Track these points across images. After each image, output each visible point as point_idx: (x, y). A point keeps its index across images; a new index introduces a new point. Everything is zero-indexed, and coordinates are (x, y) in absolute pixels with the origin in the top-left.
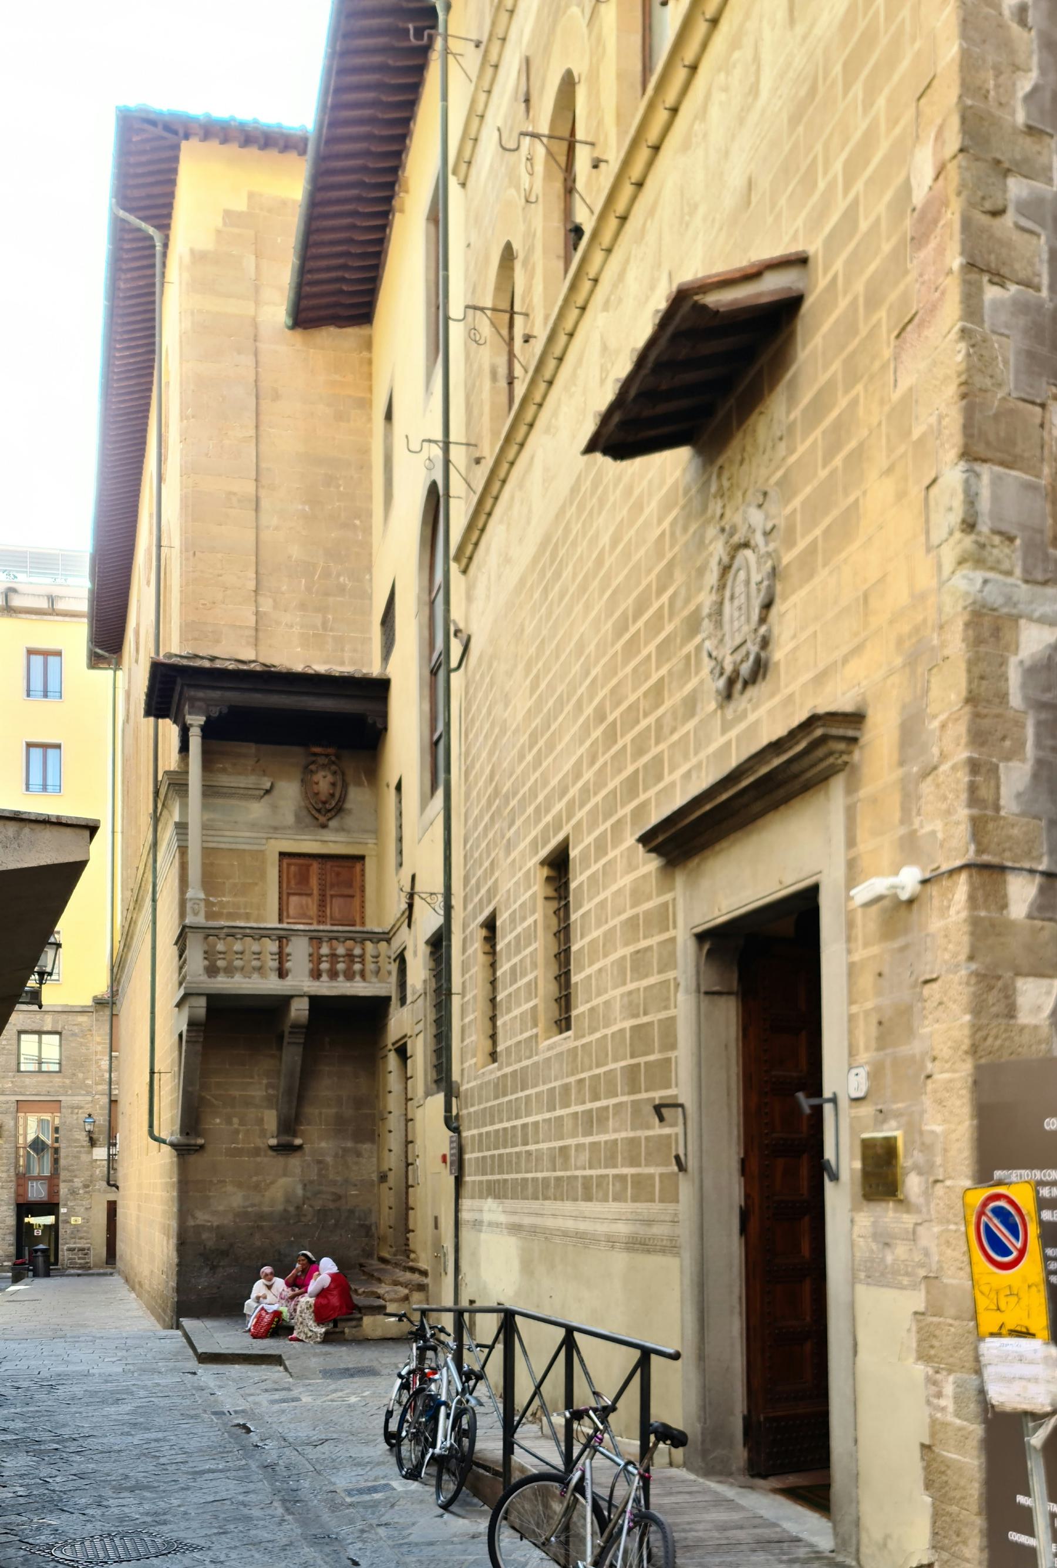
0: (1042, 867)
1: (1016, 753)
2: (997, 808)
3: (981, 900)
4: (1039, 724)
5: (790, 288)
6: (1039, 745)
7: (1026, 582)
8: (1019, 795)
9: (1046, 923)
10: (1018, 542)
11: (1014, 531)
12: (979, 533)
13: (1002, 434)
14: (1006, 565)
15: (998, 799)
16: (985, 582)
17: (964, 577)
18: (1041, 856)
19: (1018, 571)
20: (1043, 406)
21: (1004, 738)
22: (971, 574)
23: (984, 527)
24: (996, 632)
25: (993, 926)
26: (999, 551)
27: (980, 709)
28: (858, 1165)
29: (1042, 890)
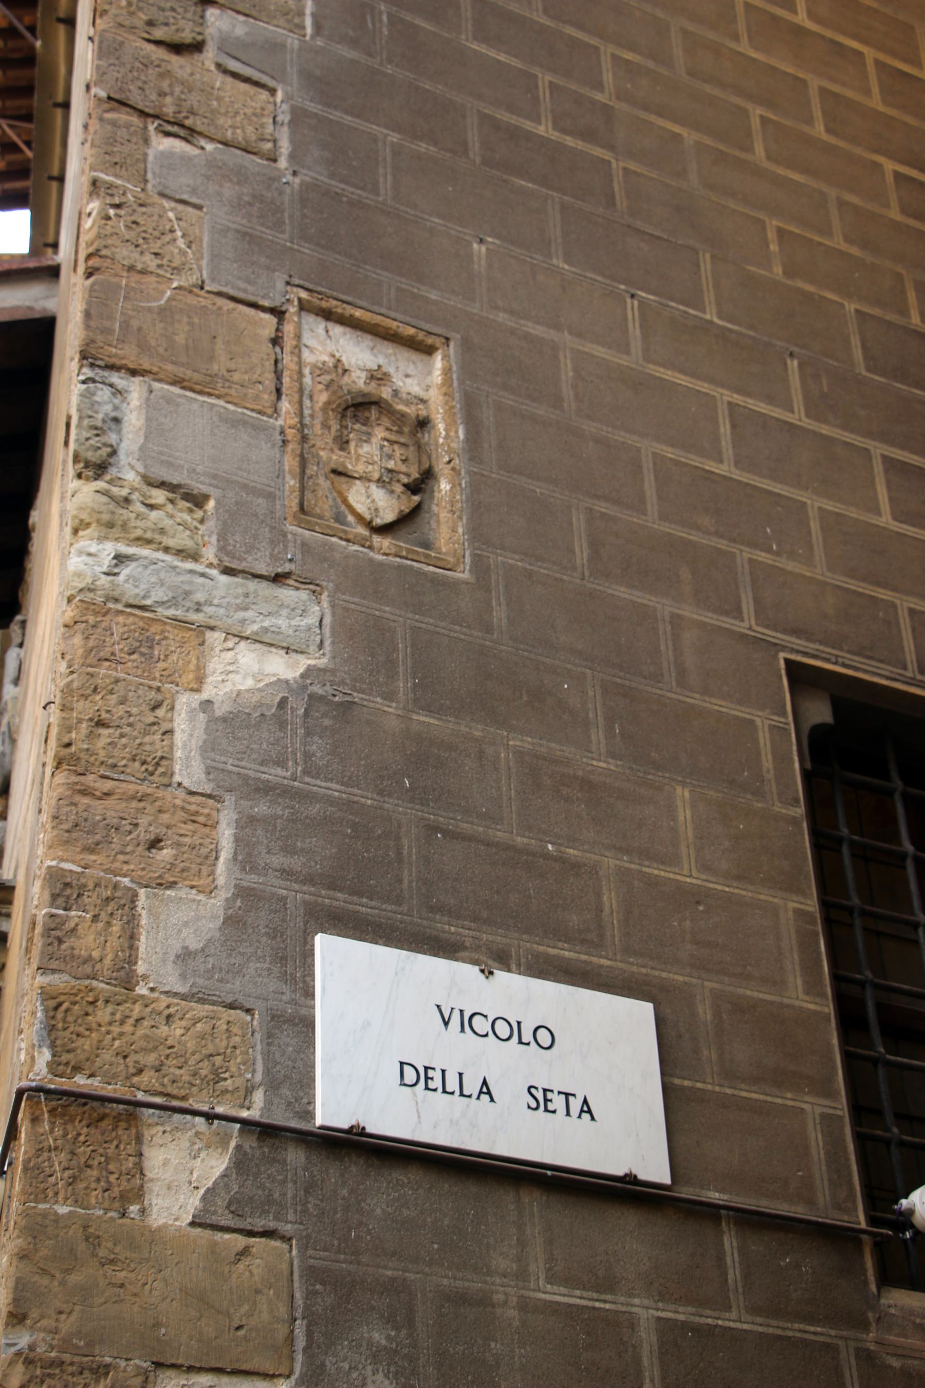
0: (252, 1114)
1: (195, 868)
2: (128, 982)
3: (60, 1177)
4: (246, 823)
5: (30, 308)
6: (245, 858)
7: (228, 571)
8: (185, 956)
9: (257, 1242)
10: (211, 504)
11: (200, 487)
12: (117, 481)
13: (180, 339)
14: (182, 539)
15: (132, 960)
16: (120, 559)
17: (80, 553)
18: (249, 1091)
19: (210, 553)
20: (278, 313)
21: (155, 844)
22: (94, 548)
23: (128, 472)
24: (144, 646)
25: (92, 1240)
26: (172, 519)
27: (90, 780)
28: (654, 1339)
29: (240, 1163)
